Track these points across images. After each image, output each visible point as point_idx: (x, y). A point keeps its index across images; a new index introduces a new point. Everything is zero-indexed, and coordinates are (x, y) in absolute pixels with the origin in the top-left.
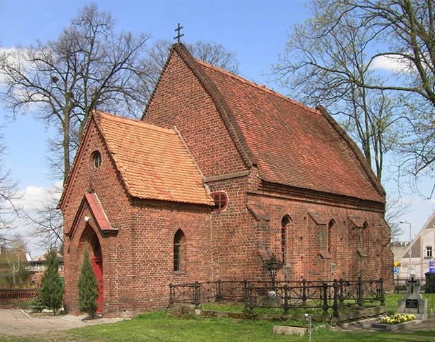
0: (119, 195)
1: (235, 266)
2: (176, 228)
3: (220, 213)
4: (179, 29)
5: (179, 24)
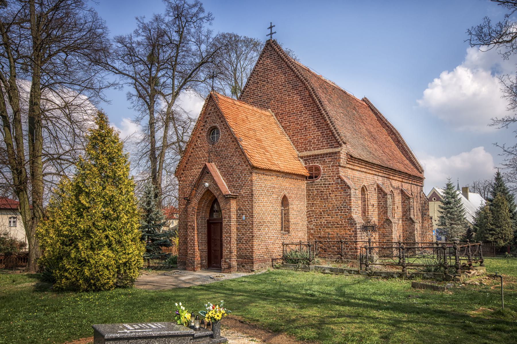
0: (239, 164)
1: (329, 227)
2: (282, 194)
3: (314, 182)
4: (271, 27)
5: (271, 23)
